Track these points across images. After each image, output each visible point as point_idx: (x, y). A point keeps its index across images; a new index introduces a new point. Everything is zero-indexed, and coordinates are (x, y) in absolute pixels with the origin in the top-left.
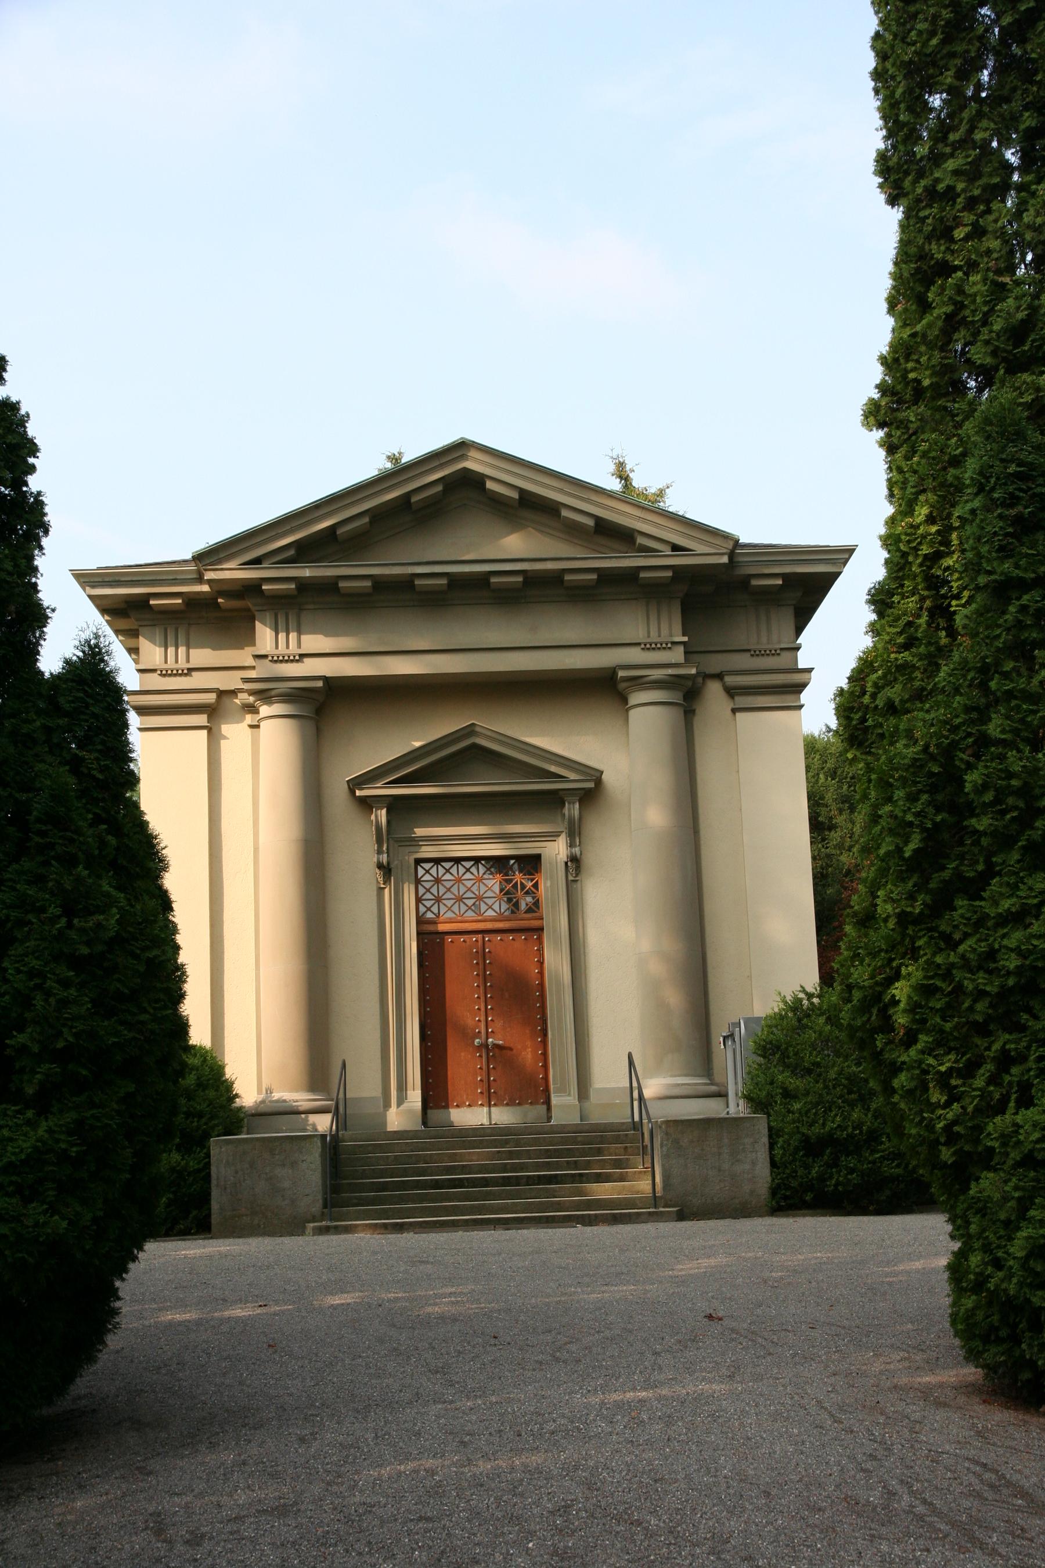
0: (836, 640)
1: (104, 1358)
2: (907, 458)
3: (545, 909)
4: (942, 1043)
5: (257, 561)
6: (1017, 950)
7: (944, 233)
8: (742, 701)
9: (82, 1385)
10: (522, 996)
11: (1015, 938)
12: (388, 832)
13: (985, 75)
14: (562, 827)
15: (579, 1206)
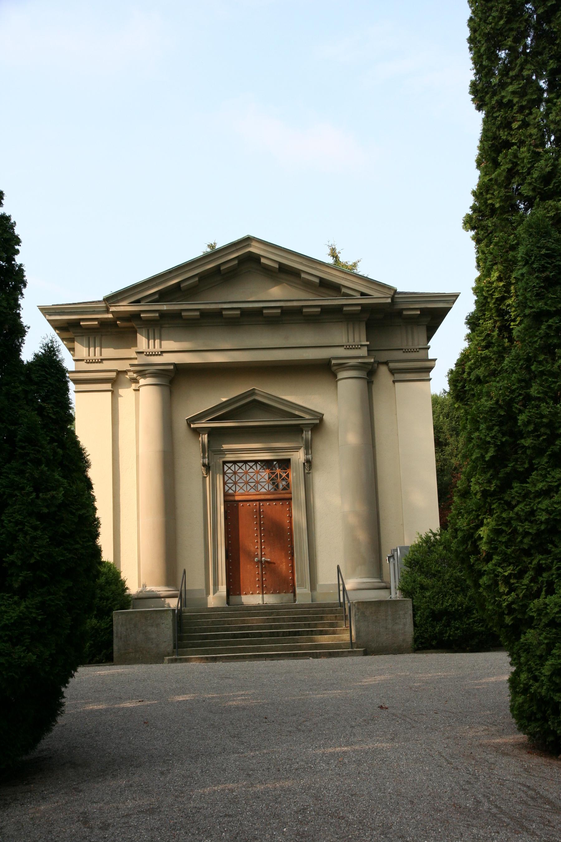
0: (449, 344)
1: (56, 729)
2: (487, 246)
3: (293, 488)
4: (506, 560)
5: (138, 301)
6: (546, 510)
7: (507, 125)
8: (398, 376)
9: (44, 744)
10: (280, 535)
11: (545, 503)
12: (209, 447)
13: (529, 40)
14: (302, 444)
15: (311, 648)
